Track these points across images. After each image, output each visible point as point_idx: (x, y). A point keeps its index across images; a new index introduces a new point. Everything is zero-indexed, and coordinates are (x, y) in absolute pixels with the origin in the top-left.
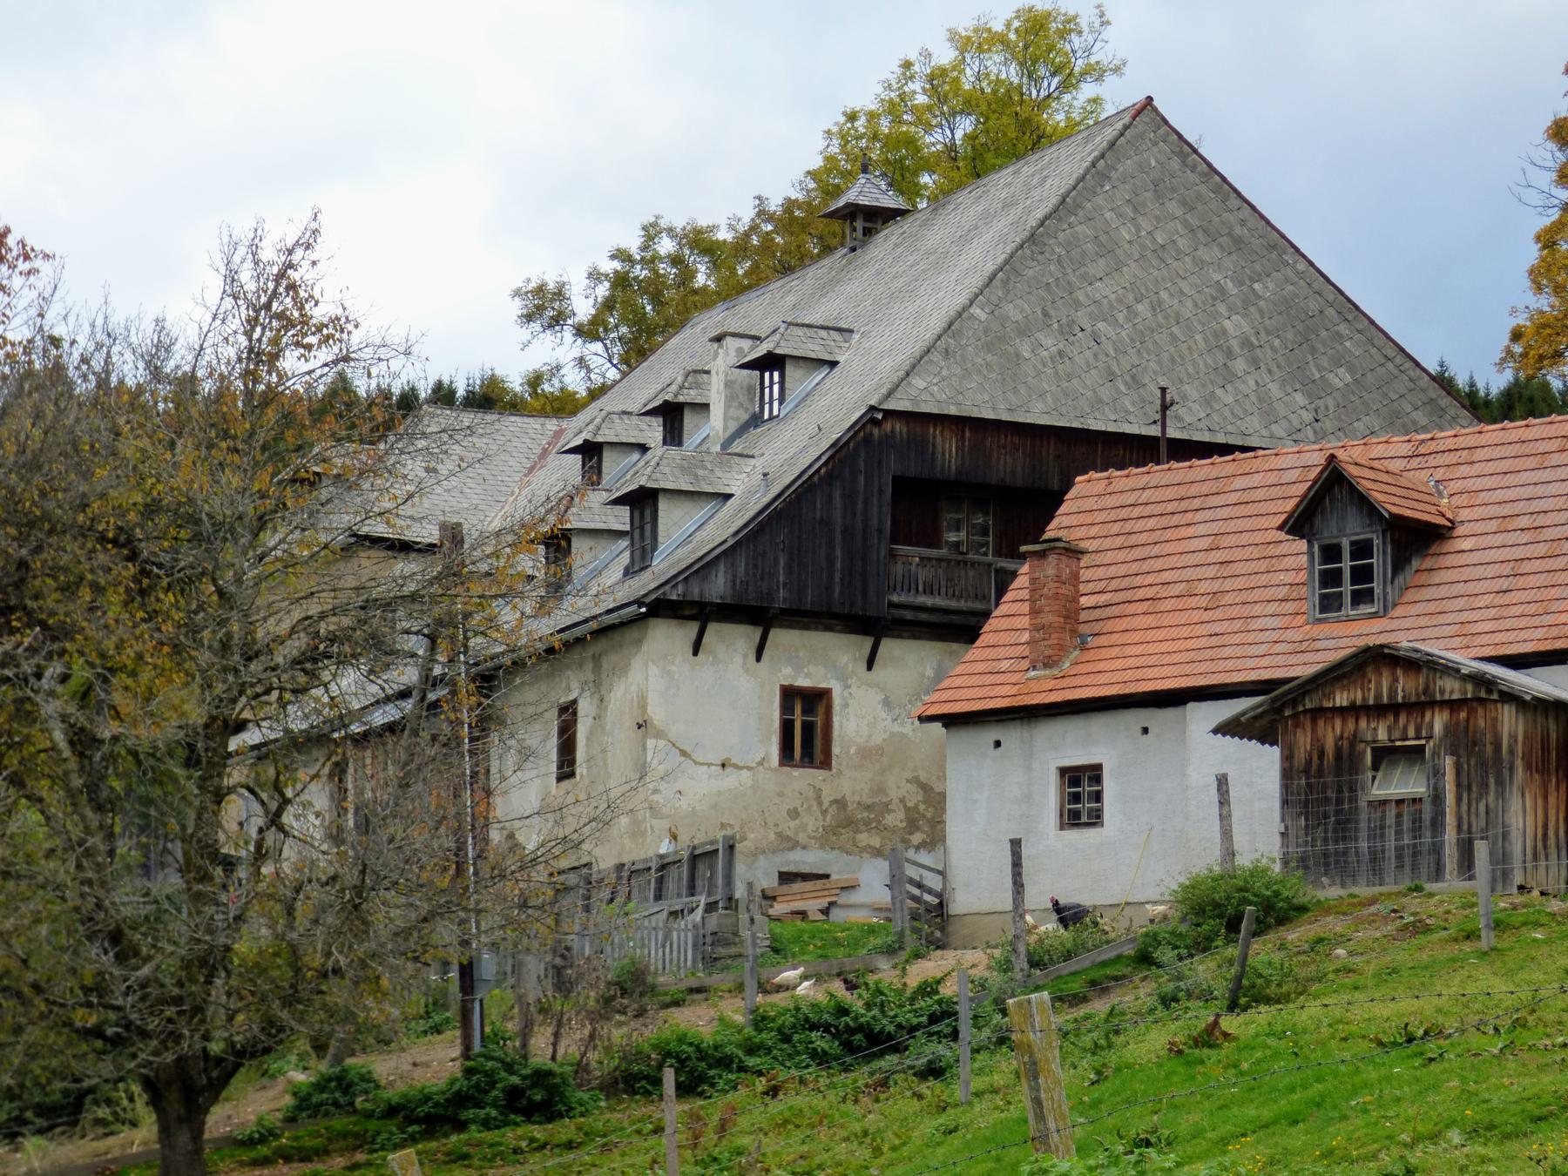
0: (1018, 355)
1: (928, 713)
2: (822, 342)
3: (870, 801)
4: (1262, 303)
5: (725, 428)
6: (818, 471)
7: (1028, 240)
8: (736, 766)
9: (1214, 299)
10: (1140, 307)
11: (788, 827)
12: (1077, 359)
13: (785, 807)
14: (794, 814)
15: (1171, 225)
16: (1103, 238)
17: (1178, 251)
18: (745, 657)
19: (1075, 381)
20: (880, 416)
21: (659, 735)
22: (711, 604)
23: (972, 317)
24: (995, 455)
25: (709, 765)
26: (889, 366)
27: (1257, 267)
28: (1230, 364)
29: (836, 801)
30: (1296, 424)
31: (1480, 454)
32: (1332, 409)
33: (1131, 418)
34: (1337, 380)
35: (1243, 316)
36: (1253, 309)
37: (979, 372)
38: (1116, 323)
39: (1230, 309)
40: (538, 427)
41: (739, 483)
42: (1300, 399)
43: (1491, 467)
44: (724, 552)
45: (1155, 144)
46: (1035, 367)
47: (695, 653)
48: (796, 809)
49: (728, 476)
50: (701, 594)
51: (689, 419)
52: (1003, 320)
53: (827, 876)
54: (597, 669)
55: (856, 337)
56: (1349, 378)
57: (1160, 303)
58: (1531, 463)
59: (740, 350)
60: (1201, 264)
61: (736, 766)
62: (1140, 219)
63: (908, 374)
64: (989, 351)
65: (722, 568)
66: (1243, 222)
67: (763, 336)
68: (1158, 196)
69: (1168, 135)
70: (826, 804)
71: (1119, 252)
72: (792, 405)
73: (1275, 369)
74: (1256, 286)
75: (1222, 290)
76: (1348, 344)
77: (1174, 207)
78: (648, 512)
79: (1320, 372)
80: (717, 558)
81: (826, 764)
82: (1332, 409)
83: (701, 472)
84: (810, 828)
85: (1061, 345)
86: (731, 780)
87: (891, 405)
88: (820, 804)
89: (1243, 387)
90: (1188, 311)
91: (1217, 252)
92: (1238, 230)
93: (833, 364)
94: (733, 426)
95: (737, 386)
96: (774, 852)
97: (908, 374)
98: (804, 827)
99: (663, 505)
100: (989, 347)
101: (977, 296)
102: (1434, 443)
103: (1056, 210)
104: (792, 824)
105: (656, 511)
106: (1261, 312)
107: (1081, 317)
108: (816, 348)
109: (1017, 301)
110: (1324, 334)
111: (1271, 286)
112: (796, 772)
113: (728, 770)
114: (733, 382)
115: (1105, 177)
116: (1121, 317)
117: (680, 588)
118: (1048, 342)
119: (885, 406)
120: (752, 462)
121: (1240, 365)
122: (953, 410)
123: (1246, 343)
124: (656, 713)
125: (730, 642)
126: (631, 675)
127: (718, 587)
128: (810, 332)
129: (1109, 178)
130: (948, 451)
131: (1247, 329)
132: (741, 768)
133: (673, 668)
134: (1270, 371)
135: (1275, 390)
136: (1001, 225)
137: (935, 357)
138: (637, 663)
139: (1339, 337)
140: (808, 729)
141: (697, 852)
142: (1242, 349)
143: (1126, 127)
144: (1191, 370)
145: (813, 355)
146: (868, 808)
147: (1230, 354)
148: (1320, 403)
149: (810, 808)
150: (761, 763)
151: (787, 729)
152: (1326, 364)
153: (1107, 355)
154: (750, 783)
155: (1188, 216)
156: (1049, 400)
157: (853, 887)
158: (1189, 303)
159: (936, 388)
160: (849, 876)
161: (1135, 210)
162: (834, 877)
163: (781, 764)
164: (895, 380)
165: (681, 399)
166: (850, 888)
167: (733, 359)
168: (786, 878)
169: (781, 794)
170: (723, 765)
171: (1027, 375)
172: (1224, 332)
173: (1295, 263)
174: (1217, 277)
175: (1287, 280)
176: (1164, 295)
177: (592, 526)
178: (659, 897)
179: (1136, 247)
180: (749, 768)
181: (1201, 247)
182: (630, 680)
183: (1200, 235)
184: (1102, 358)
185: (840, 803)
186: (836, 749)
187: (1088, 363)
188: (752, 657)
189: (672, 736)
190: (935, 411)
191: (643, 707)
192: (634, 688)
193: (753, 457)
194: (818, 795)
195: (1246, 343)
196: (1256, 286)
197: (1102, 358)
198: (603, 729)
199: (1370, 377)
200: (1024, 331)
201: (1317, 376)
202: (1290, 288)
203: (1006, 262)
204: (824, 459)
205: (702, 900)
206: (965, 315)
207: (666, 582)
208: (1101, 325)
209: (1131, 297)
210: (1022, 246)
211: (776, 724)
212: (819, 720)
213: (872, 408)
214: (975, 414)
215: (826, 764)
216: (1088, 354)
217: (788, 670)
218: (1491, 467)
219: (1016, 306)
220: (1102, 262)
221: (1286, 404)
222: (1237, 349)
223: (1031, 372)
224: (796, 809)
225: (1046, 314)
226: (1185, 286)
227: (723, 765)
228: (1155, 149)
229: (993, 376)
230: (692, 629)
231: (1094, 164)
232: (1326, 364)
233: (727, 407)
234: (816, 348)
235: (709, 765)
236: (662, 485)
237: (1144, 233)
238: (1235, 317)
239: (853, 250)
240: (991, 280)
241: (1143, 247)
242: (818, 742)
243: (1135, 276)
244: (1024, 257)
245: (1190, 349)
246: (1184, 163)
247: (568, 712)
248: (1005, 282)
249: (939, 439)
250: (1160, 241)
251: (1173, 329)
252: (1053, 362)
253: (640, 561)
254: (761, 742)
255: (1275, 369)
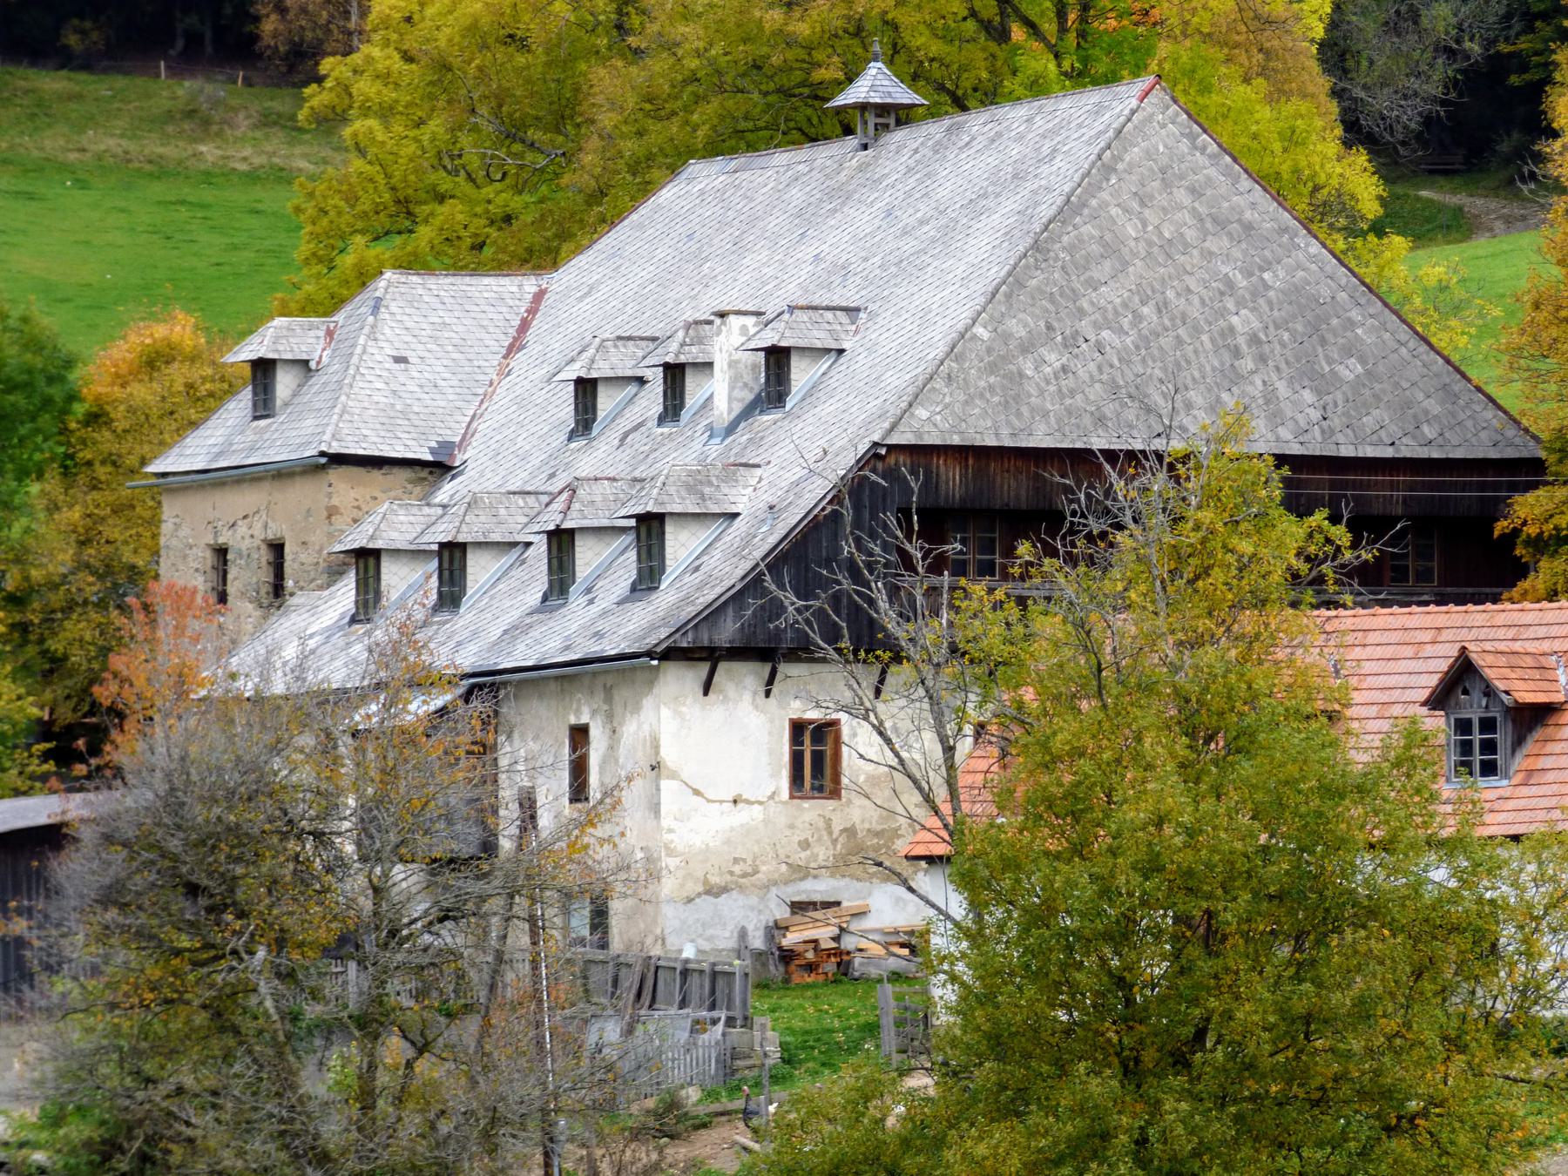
0: (1021, 375)
1: (913, 853)
2: (828, 327)
3: (879, 828)
4: (1271, 293)
5: (730, 410)
6: (823, 509)
7: (1032, 248)
8: (748, 802)
9: (1222, 294)
10: (1145, 310)
11: (801, 857)
12: (1080, 373)
13: (796, 839)
14: (805, 845)
15: (1178, 216)
16: (1108, 237)
17: (1186, 245)
18: (755, 693)
19: (1079, 397)
20: (883, 451)
21: (674, 775)
22: (721, 649)
23: (974, 337)
24: (998, 479)
25: (721, 802)
26: (899, 380)
27: (1267, 253)
28: (1237, 363)
29: (845, 830)
30: (1303, 424)
31: (1372, 638)
32: (1340, 403)
33: (1135, 433)
34: (1347, 372)
35: (1253, 310)
36: (1261, 301)
37: (982, 395)
38: (1121, 331)
39: (1238, 304)
40: (514, 289)
41: (745, 499)
42: (1308, 396)
43: (1380, 652)
44: (732, 597)
45: (1163, 126)
46: (1038, 385)
47: (706, 693)
48: (806, 840)
49: (734, 491)
50: (711, 640)
51: (691, 381)
52: (1006, 337)
53: (838, 904)
54: (609, 699)
55: (862, 315)
56: (1359, 369)
57: (1166, 304)
58: (1408, 651)
59: (744, 329)
60: (1208, 255)
61: (748, 802)
62: (1147, 212)
63: (910, 405)
64: (992, 373)
65: (730, 612)
66: (1253, 205)
67: (771, 311)
68: (1167, 185)
69: (1177, 115)
70: (836, 834)
71: (1125, 251)
72: (798, 397)
73: (1283, 366)
74: (1266, 276)
75: (1230, 284)
76: (1359, 331)
77: (1181, 196)
78: (654, 531)
79: (1329, 364)
80: (725, 603)
81: (835, 793)
82: (1340, 403)
83: (707, 490)
84: (821, 857)
85: (1064, 360)
86: (744, 815)
87: (895, 439)
88: (830, 833)
89: (1249, 389)
90: (1195, 312)
91: (1225, 242)
92: (1248, 215)
93: (841, 352)
94: (738, 408)
95: (741, 366)
96: (786, 883)
97: (910, 405)
98: (815, 857)
99: (670, 529)
100: (992, 368)
101: (979, 314)
102: (1337, 621)
103: (1060, 211)
104: (803, 855)
105: (663, 533)
106: (1270, 303)
107: (1085, 326)
108: (822, 335)
109: (1021, 316)
110: (1335, 321)
111: (1281, 274)
112: (806, 804)
113: (740, 806)
114: (737, 362)
115: (1109, 170)
116: (1126, 322)
117: (690, 636)
118: (1052, 357)
119: (889, 442)
120: (758, 472)
121: (1247, 364)
122: (956, 440)
123: (1254, 340)
124: (668, 755)
125: (740, 681)
126: (643, 713)
127: (727, 632)
128: (815, 315)
129: (1115, 170)
130: (953, 479)
131: (1256, 324)
132: (752, 803)
133: (684, 709)
134: (1278, 369)
135: (1282, 388)
136: (1004, 212)
137: (938, 384)
138: (648, 703)
139: (1351, 324)
140: (818, 758)
141: (718, 968)
142: (1250, 347)
143: (1133, 112)
144: (1197, 374)
145: (819, 345)
146: (878, 834)
147: (1237, 353)
148: (1328, 398)
149: (819, 840)
150: (771, 797)
151: (797, 760)
152: (1336, 356)
153: (1112, 366)
154: (761, 817)
155: (1196, 205)
156: (1053, 420)
157: (864, 913)
158: (1196, 301)
159: (938, 417)
160: (860, 902)
161: (1143, 204)
162: (845, 904)
163: (792, 797)
164: (899, 412)
165: (682, 359)
166: (861, 914)
167: (737, 340)
168: (798, 907)
169: (792, 827)
170: (735, 802)
171: (1030, 396)
172: (1232, 329)
173: (1307, 245)
174: (1225, 269)
175: (1299, 267)
176: (1170, 294)
177: (596, 523)
178: (683, 1004)
179: (1142, 244)
180: (761, 803)
181: (1210, 238)
182: (642, 718)
183: (1209, 225)
184: (1107, 369)
185: (850, 832)
186: (845, 781)
187: (1092, 377)
188: (762, 690)
189: (684, 776)
190: (938, 442)
191: (656, 747)
192: (646, 727)
193: (758, 466)
194: (828, 823)
195: (1254, 340)
196: (1266, 276)
197: (1107, 369)
198: (617, 761)
199: (1381, 368)
200: (1026, 348)
201: (1327, 369)
202: (1301, 274)
203: (1009, 274)
204: (829, 497)
205: (723, 1015)
206: (968, 336)
207: (677, 630)
208: (1106, 334)
209: (1136, 299)
210: (1025, 255)
211: (786, 757)
212: (828, 749)
213: (876, 444)
214: (979, 441)
215: (835, 793)
216: (1092, 366)
217: (797, 704)
218: (1380, 652)
219: (1020, 321)
220: (1107, 264)
221: (1294, 403)
222: (1244, 347)
223: (1034, 392)
224: (806, 840)
225: (1049, 327)
226: (1192, 282)
227: (735, 802)
228: (1163, 132)
229: (996, 399)
230: (704, 668)
231: (1099, 157)
232: (1336, 356)
233: (732, 388)
234: (822, 335)
235: (721, 802)
236: (668, 509)
237: (1150, 228)
238: (1243, 312)
239: (865, 147)
240: (994, 295)
241: (1150, 244)
242: (828, 771)
243: (1141, 277)
244: (1027, 267)
245: (1196, 351)
246: (1193, 143)
247: (579, 735)
248: (1008, 296)
249: (942, 469)
250: (1167, 235)
251: (1180, 331)
252: (1057, 378)
253: (649, 577)
254: (772, 776)
255: (1283, 366)
